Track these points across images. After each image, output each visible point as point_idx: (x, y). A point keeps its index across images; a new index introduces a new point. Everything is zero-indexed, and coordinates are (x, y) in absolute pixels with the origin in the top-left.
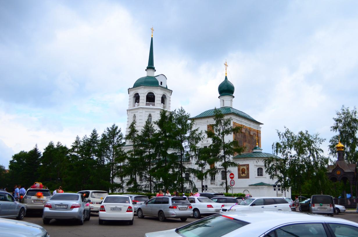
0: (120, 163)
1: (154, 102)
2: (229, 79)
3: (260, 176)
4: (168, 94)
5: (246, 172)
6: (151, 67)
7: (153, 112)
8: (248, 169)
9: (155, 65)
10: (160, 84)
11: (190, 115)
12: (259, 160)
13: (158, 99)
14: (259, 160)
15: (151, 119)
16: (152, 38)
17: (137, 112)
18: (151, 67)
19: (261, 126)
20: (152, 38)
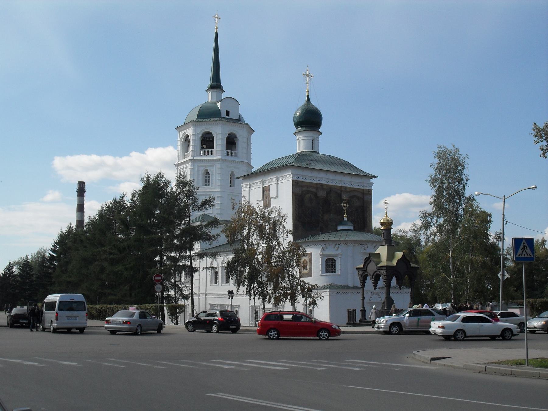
0: (513, 261)
1: (213, 147)
2: (313, 102)
3: (332, 272)
4: (240, 133)
5: (308, 267)
6: (216, 84)
7: (211, 166)
8: (311, 261)
9: (223, 83)
10: (224, 115)
11: (536, 139)
12: (328, 246)
13: (219, 143)
14: (328, 246)
15: (209, 177)
16: (217, 33)
17: (213, 166)
18: (216, 84)
19: (372, 180)
20: (217, 33)
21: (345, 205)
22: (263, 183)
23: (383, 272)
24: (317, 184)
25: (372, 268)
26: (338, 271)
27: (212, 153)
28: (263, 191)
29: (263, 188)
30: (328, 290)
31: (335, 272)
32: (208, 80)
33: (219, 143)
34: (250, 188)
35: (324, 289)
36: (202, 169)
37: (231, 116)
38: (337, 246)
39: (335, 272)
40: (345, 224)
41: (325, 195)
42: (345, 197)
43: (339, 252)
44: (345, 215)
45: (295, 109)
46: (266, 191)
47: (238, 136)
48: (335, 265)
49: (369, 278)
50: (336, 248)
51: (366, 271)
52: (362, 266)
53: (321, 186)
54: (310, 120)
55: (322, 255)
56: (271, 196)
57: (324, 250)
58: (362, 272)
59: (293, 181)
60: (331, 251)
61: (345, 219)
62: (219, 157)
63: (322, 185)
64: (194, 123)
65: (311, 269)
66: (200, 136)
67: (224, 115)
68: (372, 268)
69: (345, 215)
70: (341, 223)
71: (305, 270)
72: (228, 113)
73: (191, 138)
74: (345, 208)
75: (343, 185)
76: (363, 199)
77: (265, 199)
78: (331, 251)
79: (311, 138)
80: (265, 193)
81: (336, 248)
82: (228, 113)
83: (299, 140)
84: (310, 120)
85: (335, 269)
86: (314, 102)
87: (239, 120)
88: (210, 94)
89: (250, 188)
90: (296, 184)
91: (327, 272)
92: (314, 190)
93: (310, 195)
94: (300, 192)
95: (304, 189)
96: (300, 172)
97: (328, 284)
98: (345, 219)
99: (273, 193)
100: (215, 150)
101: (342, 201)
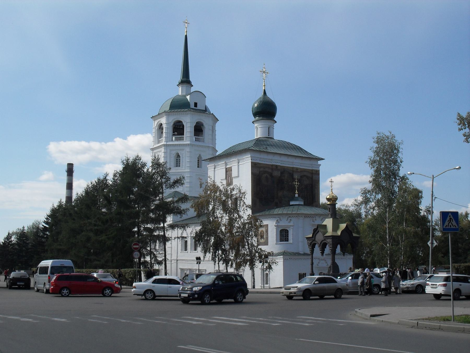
2: (269, 95)
5: (265, 237)
6: (186, 80)
8: (267, 231)
10: (192, 106)
13: (188, 130)
14: (281, 217)
16: (186, 36)
18: (186, 80)
19: (320, 162)
20: (186, 36)
21: (296, 183)
22: (226, 164)
23: (329, 241)
24: (272, 165)
25: (319, 237)
26: (291, 241)
27: (182, 139)
28: (226, 172)
29: (226, 169)
30: (282, 257)
31: (288, 241)
32: (179, 76)
33: (188, 130)
34: (215, 168)
35: (278, 255)
36: (174, 153)
37: (199, 107)
38: (290, 218)
39: (288, 241)
40: (296, 199)
41: (279, 175)
42: (296, 176)
43: (291, 224)
44: (297, 192)
45: (254, 100)
46: (228, 171)
47: (204, 125)
48: (288, 235)
49: (317, 246)
50: (289, 221)
51: (314, 240)
52: (311, 236)
53: (276, 167)
54: (266, 111)
55: (277, 226)
56: (233, 176)
57: (279, 222)
58: (311, 241)
59: (252, 162)
60: (284, 223)
61: (297, 195)
62: (189, 143)
63: (277, 166)
64: (167, 113)
65: (267, 238)
66: (172, 124)
67: (192, 106)
68: (319, 237)
69: (297, 192)
70: (293, 199)
71: (262, 239)
72: (196, 105)
73: (164, 126)
74: (296, 186)
75: (294, 166)
76: (312, 178)
77: (227, 178)
78: (284, 223)
79: (267, 126)
80: (228, 173)
81: (289, 221)
82: (196, 105)
83: (257, 128)
84: (266, 111)
85: (288, 239)
86: (270, 95)
87: (205, 111)
88: (180, 88)
89: (215, 168)
90: (254, 165)
91: (281, 241)
92: (270, 171)
93: (266, 175)
94: (258, 173)
95: (262, 169)
96: (257, 155)
97: (282, 251)
98: (297, 195)
99: (234, 173)
100: (185, 136)
101: (294, 180)
